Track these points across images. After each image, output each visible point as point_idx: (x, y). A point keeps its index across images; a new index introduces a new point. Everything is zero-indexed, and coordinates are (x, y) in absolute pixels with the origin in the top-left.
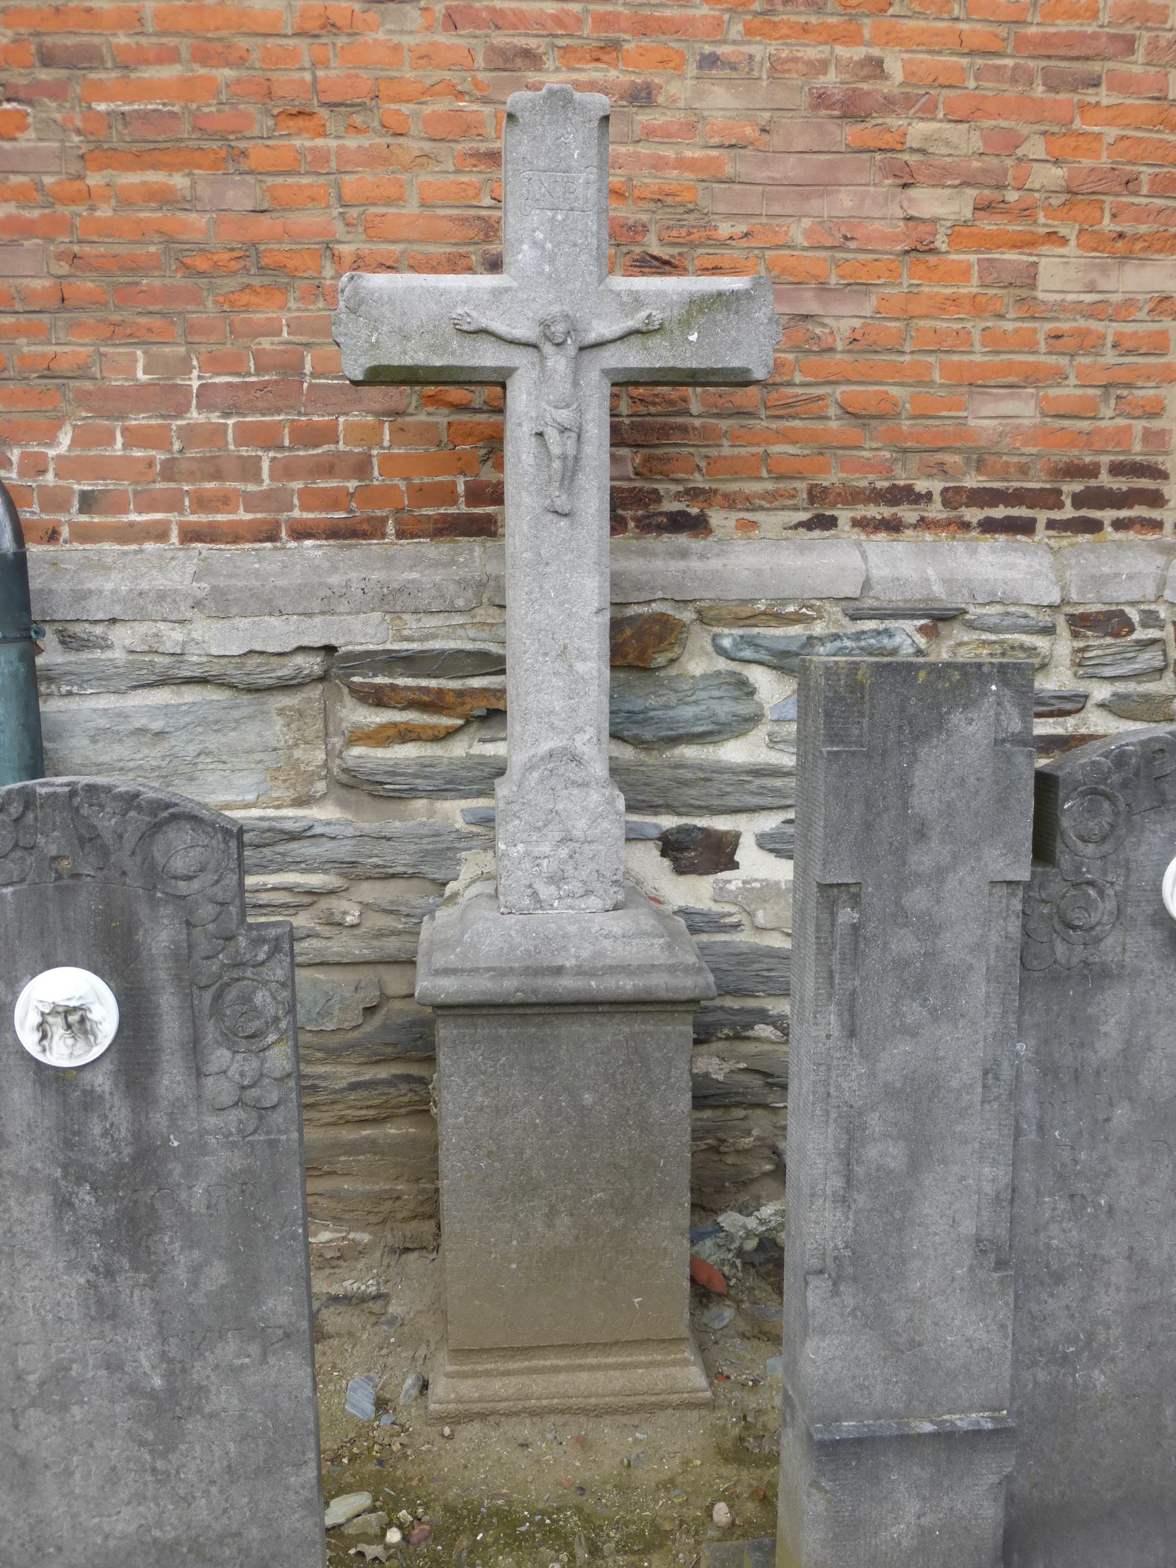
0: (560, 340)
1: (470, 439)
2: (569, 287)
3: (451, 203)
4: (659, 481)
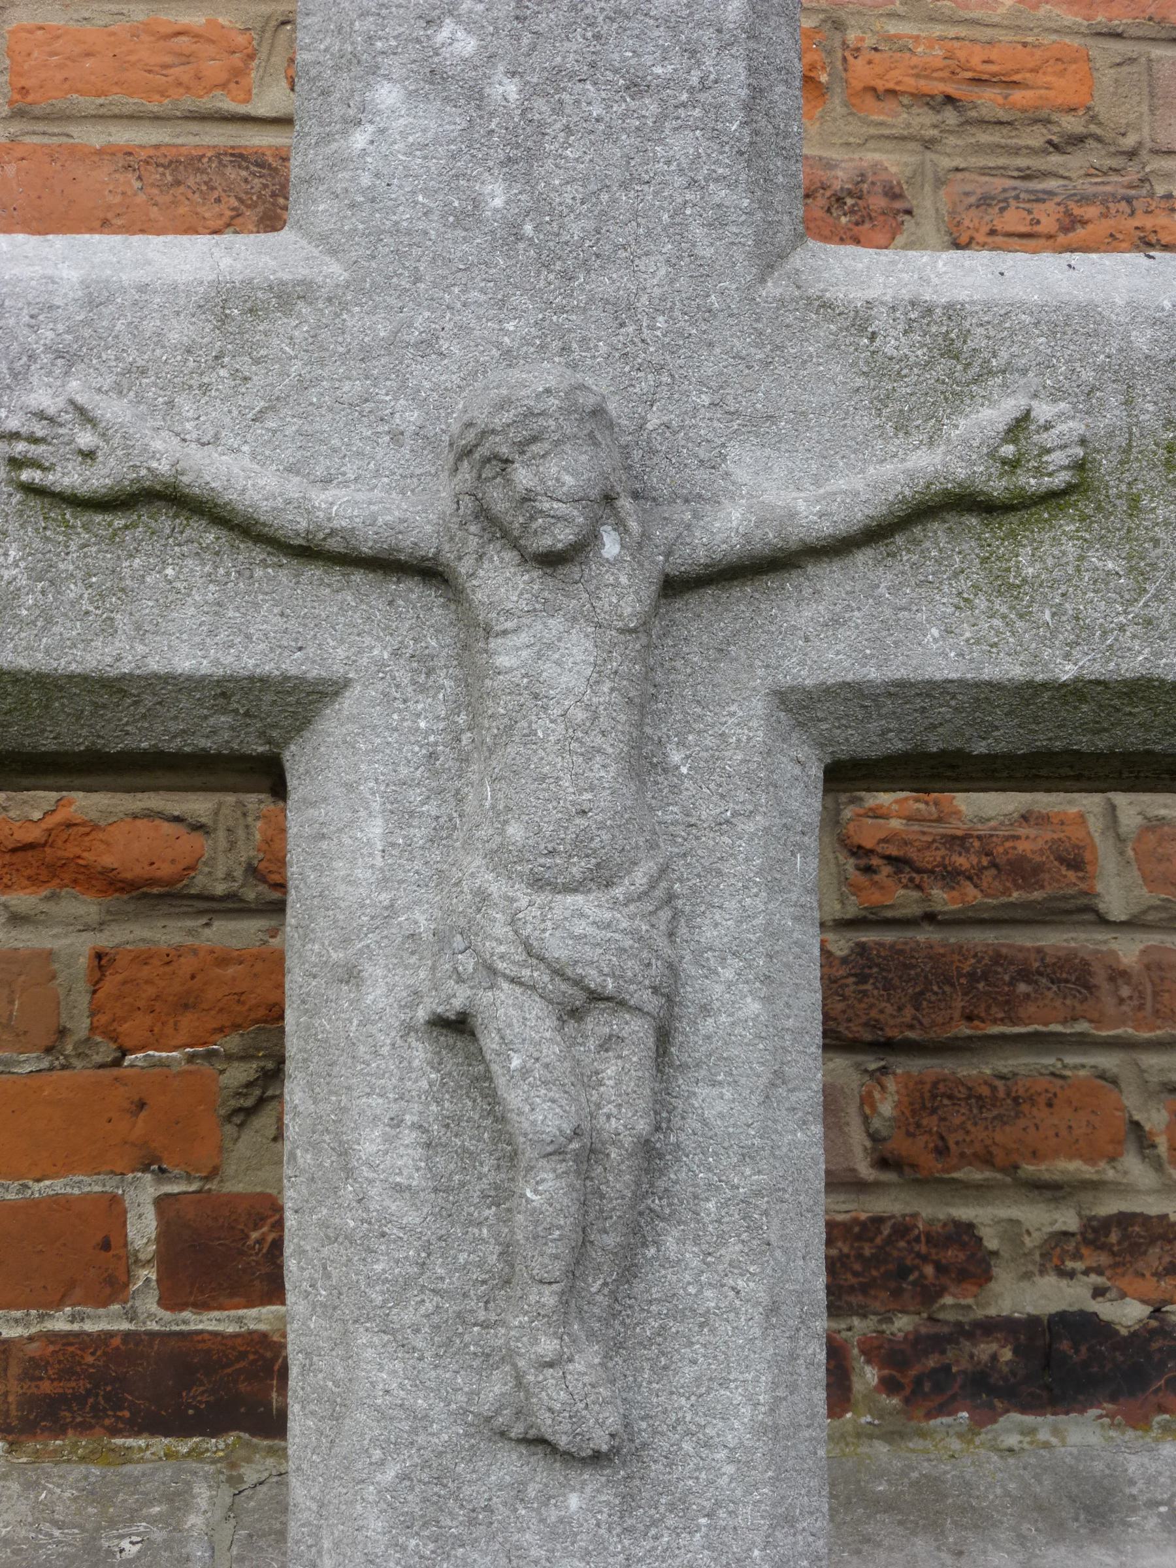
0: (563, 536)
1: (187, 1021)
2: (605, 284)
3: (131, 103)
4: (980, 1191)
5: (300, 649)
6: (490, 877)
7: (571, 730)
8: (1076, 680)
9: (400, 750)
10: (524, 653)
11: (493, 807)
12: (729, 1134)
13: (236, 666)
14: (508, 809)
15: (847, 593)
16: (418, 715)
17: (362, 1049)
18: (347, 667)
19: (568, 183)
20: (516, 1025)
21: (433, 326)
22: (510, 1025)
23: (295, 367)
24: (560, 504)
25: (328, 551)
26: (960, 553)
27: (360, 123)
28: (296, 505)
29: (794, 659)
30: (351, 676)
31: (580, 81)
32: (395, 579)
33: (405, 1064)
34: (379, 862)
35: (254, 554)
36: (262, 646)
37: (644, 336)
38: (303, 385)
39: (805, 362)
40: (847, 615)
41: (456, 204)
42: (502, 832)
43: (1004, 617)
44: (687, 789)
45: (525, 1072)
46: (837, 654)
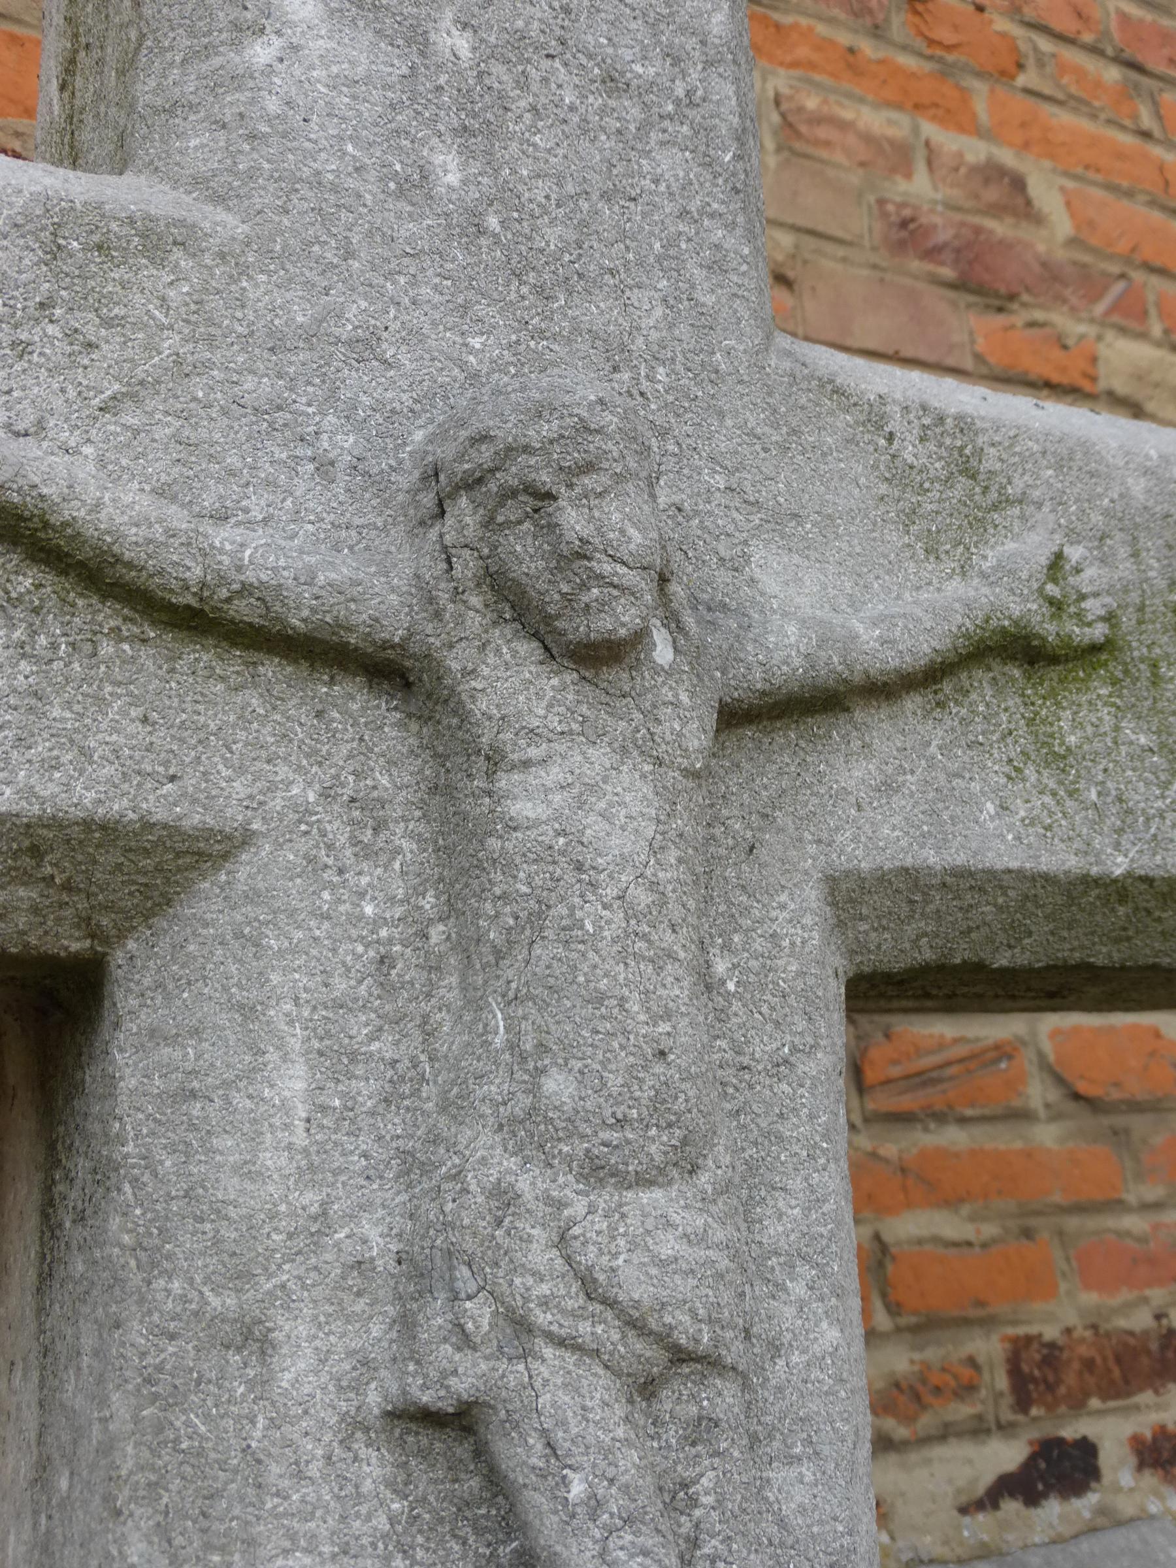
5: (172, 779)
6: (512, 1163)
7: (633, 922)
8: (1129, 874)
9: (334, 951)
10: (557, 798)
11: (512, 1046)
12: (813, 1536)
13: (63, 800)
14: (542, 1048)
15: (898, 750)
16: (362, 895)
17: (275, 1469)
18: (249, 813)
19: (539, 176)
20: (572, 1422)
21: (373, 322)
22: (563, 1424)
23: (170, 343)
24: (626, 570)
25: (232, 621)
26: (1006, 710)
27: (262, 30)
28: (183, 540)
29: (848, 834)
30: (255, 826)
31: (548, 56)
32: (326, 677)
33: (350, 1489)
34: (300, 1139)
35: (100, 618)
36: (108, 770)
37: (643, 388)
38: (181, 369)
39: (824, 454)
40: (900, 779)
41: (398, 167)
42: (534, 1089)
43: (1054, 794)
44: (736, 1015)
45: (595, 1505)
46: (893, 830)
